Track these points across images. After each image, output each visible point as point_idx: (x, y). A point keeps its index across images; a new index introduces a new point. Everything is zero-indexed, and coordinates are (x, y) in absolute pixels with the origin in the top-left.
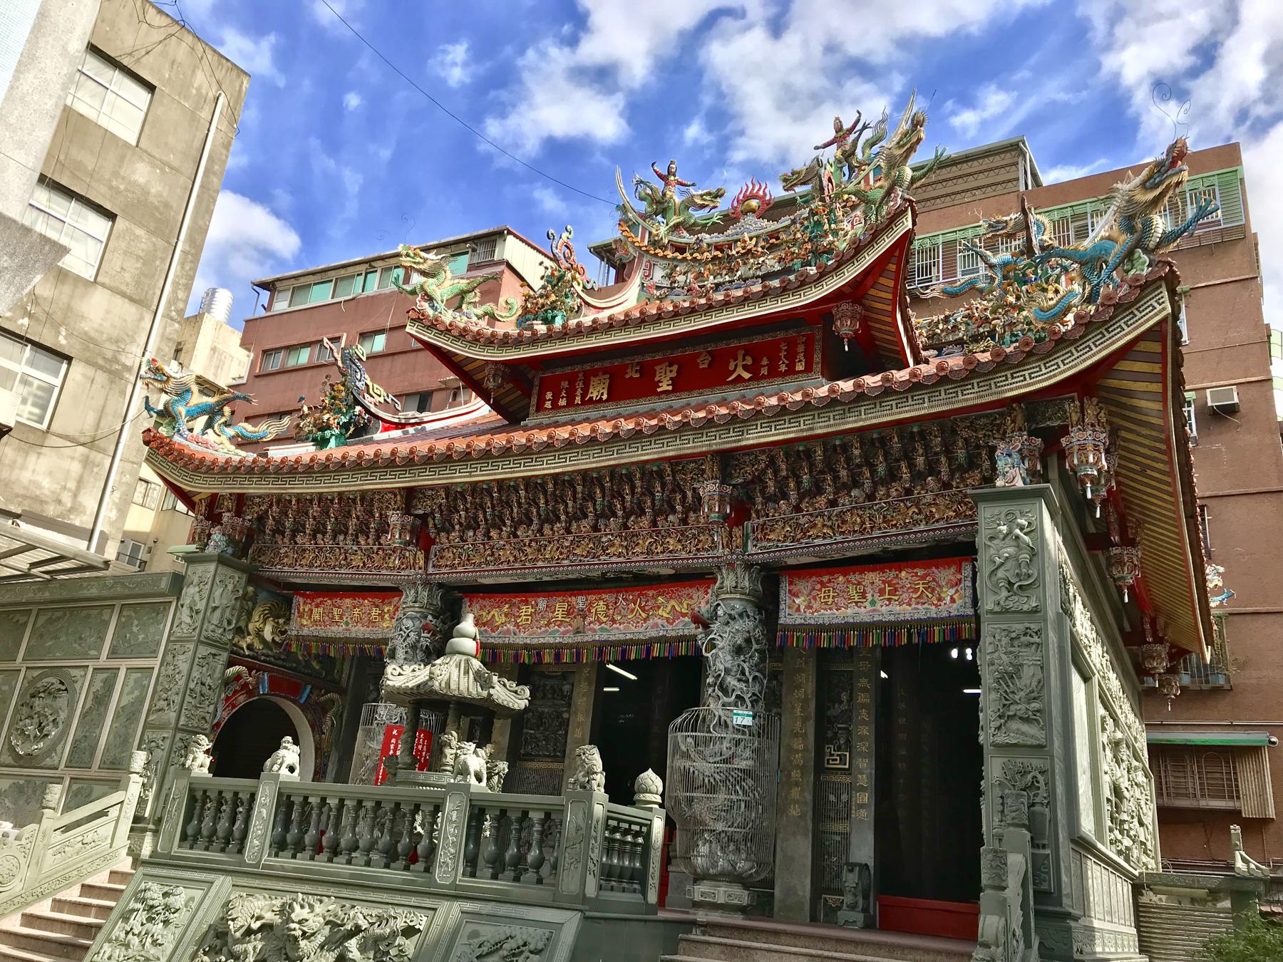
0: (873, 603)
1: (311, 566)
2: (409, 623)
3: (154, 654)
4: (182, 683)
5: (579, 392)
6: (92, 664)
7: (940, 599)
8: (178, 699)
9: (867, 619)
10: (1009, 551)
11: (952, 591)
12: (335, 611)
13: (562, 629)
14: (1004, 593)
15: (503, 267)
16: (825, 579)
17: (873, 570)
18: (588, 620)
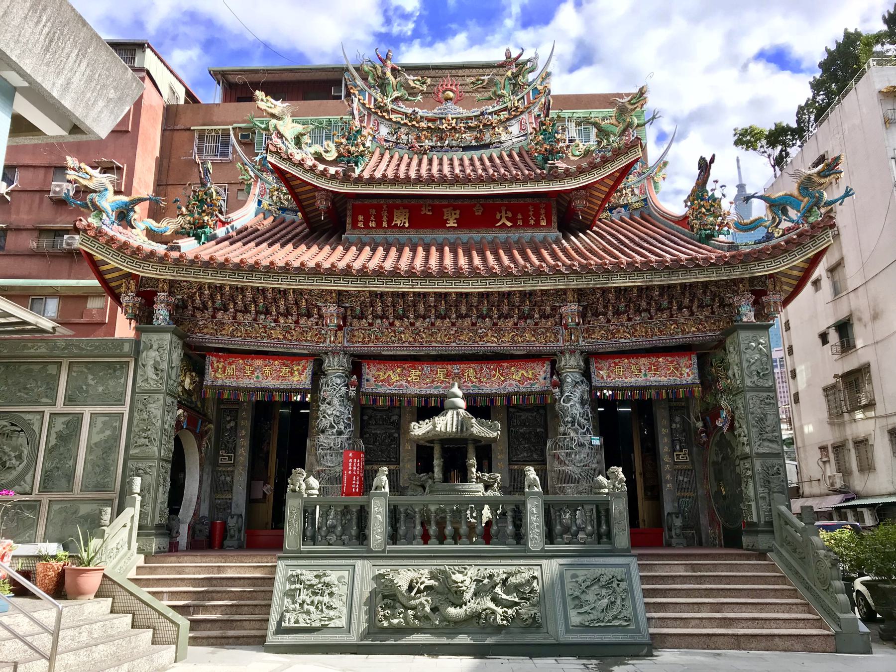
0: (645, 375)
1: (233, 336)
2: (339, 381)
3: (120, 401)
4: (158, 424)
5: (385, 218)
6: (48, 410)
7: (681, 374)
8: (157, 437)
9: (643, 384)
10: (757, 356)
11: (688, 370)
12: (247, 368)
13: (443, 385)
14: (756, 378)
15: (144, 74)
16: (617, 361)
17: (644, 357)
18: (462, 380)
